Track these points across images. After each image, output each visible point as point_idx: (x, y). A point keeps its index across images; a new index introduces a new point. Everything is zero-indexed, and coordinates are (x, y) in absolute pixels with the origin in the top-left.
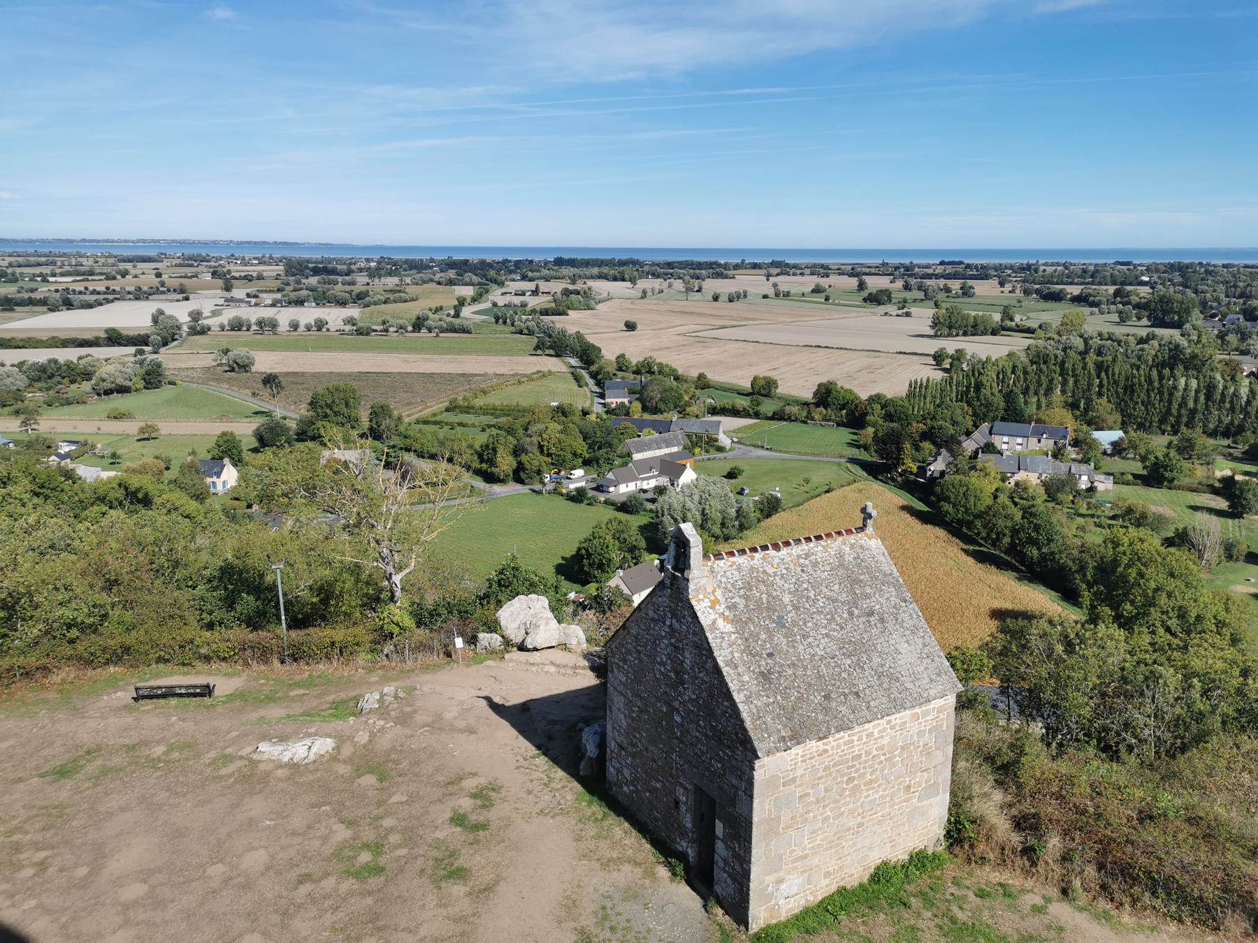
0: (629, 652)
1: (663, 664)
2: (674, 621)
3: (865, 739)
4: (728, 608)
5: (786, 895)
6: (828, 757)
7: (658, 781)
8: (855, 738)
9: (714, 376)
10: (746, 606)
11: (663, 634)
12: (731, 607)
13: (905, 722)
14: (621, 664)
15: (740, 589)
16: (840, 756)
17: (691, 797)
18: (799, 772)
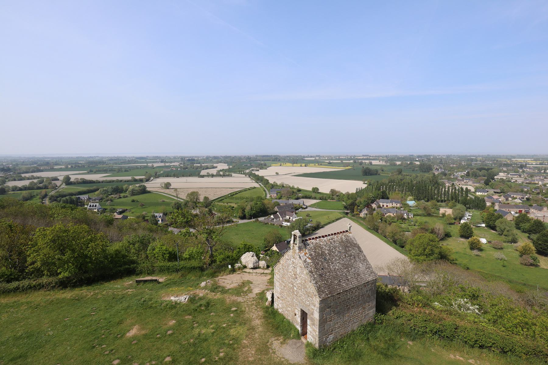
1: (290, 272)
2: (294, 259)
4: (310, 255)
5: (329, 341)
7: (290, 308)
8: (348, 293)
9: (301, 187)
10: (315, 254)
12: (311, 255)
15: (313, 249)
17: (300, 313)
18: (332, 304)
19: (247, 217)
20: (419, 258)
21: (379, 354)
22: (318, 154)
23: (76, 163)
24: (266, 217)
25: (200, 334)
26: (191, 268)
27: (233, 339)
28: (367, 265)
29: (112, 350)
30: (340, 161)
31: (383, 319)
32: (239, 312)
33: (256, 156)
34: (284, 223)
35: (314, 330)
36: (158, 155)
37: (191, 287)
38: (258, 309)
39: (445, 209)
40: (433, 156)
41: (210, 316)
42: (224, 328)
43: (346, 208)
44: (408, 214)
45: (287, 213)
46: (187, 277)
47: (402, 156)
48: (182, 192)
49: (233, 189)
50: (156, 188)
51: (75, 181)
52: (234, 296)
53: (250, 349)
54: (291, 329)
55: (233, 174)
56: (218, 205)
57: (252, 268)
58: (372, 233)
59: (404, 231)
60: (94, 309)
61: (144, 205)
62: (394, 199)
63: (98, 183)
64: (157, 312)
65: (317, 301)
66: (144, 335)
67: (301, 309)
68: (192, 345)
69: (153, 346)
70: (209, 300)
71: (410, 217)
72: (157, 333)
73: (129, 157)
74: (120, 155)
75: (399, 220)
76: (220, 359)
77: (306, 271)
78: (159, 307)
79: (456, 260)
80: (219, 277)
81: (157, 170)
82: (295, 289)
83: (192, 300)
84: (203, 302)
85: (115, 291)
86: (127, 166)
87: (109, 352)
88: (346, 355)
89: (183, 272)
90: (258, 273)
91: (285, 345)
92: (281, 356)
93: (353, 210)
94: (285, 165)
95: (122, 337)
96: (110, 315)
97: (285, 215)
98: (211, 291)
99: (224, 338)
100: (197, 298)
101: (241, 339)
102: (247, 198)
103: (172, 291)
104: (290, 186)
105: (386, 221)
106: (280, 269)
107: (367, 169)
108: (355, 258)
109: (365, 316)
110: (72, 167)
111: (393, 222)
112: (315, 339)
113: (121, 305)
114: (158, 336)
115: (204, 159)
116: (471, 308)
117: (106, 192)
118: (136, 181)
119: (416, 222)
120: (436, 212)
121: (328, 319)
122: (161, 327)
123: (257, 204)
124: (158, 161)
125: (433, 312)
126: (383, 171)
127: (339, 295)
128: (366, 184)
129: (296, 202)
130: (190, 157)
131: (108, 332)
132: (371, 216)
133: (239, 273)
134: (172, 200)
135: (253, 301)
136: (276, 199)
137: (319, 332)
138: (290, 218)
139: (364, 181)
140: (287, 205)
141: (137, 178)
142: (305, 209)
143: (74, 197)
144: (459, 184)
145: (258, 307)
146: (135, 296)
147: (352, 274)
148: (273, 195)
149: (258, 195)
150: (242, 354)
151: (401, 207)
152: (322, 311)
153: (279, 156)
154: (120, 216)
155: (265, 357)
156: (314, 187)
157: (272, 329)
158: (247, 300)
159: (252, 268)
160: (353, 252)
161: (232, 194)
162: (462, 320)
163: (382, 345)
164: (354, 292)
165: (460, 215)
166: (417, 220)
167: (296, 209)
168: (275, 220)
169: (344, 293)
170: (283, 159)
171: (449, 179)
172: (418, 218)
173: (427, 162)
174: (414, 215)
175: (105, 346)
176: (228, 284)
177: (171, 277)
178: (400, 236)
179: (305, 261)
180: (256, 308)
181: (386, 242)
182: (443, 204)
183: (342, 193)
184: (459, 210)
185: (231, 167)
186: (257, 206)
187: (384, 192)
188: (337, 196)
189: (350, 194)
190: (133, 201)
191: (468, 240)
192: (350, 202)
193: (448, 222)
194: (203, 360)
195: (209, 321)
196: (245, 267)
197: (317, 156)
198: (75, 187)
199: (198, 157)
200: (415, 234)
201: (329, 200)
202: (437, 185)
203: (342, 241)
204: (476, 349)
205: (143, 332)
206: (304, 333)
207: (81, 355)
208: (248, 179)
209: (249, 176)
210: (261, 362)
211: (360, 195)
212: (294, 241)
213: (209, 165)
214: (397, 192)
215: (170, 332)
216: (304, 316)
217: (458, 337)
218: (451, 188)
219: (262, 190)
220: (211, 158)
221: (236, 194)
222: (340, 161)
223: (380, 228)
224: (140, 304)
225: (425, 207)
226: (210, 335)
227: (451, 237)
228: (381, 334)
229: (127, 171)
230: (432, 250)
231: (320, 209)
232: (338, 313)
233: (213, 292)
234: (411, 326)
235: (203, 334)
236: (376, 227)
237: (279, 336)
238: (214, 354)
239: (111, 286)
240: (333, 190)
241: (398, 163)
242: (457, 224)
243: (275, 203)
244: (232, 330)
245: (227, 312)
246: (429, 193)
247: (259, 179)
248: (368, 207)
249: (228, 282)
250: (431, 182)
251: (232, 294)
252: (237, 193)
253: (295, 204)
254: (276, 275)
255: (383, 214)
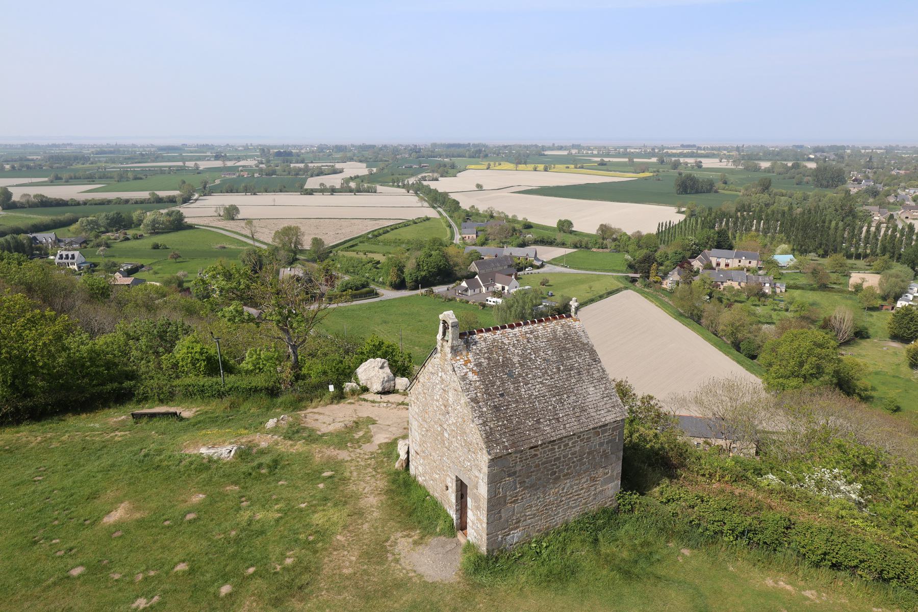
0: (419, 393)
1: (437, 401)
2: (443, 373)
3: (562, 448)
4: (476, 365)
6: (538, 458)
7: (437, 474)
8: (556, 447)
9: (532, 220)
10: (488, 364)
11: (437, 382)
12: (479, 365)
13: (590, 437)
14: (416, 401)
15: (485, 353)
16: (546, 458)
18: (518, 468)
19: (408, 285)
20: (785, 381)
21: (612, 570)
22: (576, 143)
23: (21, 159)
24: (451, 286)
25: (251, 521)
26: (250, 389)
27: (316, 532)
28: (606, 390)
29: (71, 550)
30: (626, 160)
31: (635, 503)
32: (336, 480)
33: (432, 145)
34: (489, 298)
35: (479, 519)
36: (209, 142)
37: (246, 429)
38: (379, 476)
39: (862, 275)
40: (853, 148)
41: (276, 487)
42: (301, 510)
43: (631, 267)
44: (775, 284)
45: (498, 276)
46: (242, 409)
47: (777, 147)
48: (266, 227)
49: (377, 222)
50: (205, 219)
51: (24, 200)
52: (331, 448)
53: (349, 552)
54: (438, 517)
55: (379, 188)
56: (344, 256)
57: (378, 393)
58: (687, 325)
59: (760, 322)
60: (41, 469)
61: (180, 257)
62: (744, 249)
63: (75, 205)
64: (170, 477)
65: (484, 459)
66: (137, 521)
67: (457, 477)
68: (232, 542)
69: (155, 542)
70: (279, 455)
71: (778, 290)
72: (164, 517)
73: (143, 147)
74: (121, 142)
75: (752, 298)
76: (284, 569)
77: (464, 399)
78: (174, 467)
79: (873, 389)
80: (309, 410)
81: (206, 176)
82: (446, 435)
83: (244, 454)
84: (267, 459)
85: (87, 434)
86: (138, 167)
87: (65, 553)
88: (544, 570)
89: (232, 398)
90: (393, 403)
91: (420, 547)
92: (409, 568)
93: (648, 272)
94: (499, 167)
95: (93, 523)
96: (74, 482)
97: (494, 281)
98: (285, 438)
99: (298, 529)
100: (255, 450)
101: (333, 533)
102: (409, 242)
103: (205, 435)
104: (506, 217)
105: (720, 300)
106: (419, 393)
107: (690, 178)
108: (579, 373)
109: (595, 494)
110: (13, 167)
111: (736, 301)
112: (481, 536)
113: (97, 463)
114: (167, 523)
115: (313, 152)
116: (842, 488)
117: (94, 225)
118: (159, 200)
119: (791, 303)
120: (841, 281)
121: (509, 498)
122: (175, 506)
123: (431, 256)
124: (208, 156)
125: (752, 493)
126: (725, 183)
127: (535, 451)
128: (683, 213)
129: (519, 253)
130: (283, 147)
131: (67, 515)
132: (687, 287)
133: (353, 401)
134: (243, 246)
135: (370, 459)
136: (475, 245)
137: (488, 523)
138: (503, 288)
139: (679, 207)
140: (498, 260)
141: (162, 194)
142: (538, 268)
143: (22, 237)
144: (907, 218)
145: (379, 471)
146: (128, 443)
147: (569, 408)
148: (467, 236)
149: (434, 236)
150: (331, 561)
151: (760, 269)
152: (493, 481)
153: (486, 146)
154: (129, 280)
155: (377, 567)
156: (563, 219)
157: (400, 515)
158: (359, 457)
159: (378, 393)
160: (577, 361)
161: (376, 233)
162: (813, 511)
163: (625, 554)
164: (570, 445)
165: (897, 290)
166: (793, 299)
167: (518, 268)
168: (470, 292)
169: (548, 446)
170: (494, 153)
171: (882, 205)
172: (797, 293)
173: (834, 163)
174: (788, 287)
175: (58, 541)
176: (324, 423)
177: (209, 408)
178: (750, 332)
179: (464, 378)
180: (374, 473)
181: (716, 345)
182: (861, 263)
183: (625, 234)
184: (897, 276)
185: (375, 170)
186: (431, 259)
187: (721, 233)
188: (615, 240)
189: (642, 236)
190: (156, 247)
191: (908, 346)
192: (644, 252)
193: (866, 304)
194: (251, 570)
195: (274, 497)
196: (365, 390)
197: (574, 146)
198: (25, 215)
199: (301, 147)
200: (783, 329)
201: (594, 250)
202: (851, 218)
203: (555, 338)
204: (824, 571)
205: (138, 515)
206: (463, 527)
207: (9, 558)
208: (412, 199)
209: (416, 193)
210: (366, 578)
211: (666, 239)
212: (444, 334)
213: (324, 165)
214: (753, 233)
215: (190, 516)
216: (462, 490)
217: (789, 544)
218: (885, 225)
219: (444, 225)
220: (329, 148)
221: (384, 233)
222: (626, 160)
223: (705, 314)
224: (136, 460)
225: (815, 270)
226: (271, 523)
227: (868, 337)
228: (627, 531)
229: (138, 177)
230: (818, 367)
231: (573, 268)
232: (533, 487)
233: (290, 438)
234: (691, 519)
235: (258, 521)
236: (695, 312)
237: (413, 529)
238: (273, 559)
239: (81, 425)
240: (605, 226)
241: (765, 165)
242: (887, 309)
243: (471, 254)
244: (316, 515)
245: (312, 480)
246: (828, 235)
247: (438, 199)
248: (682, 266)
249: (324, 421)
250: (836, 210)
251: (328, 444)
252: (388, 232)
253: (515, 257)
254: (413, 405)
255: (716, 282)
